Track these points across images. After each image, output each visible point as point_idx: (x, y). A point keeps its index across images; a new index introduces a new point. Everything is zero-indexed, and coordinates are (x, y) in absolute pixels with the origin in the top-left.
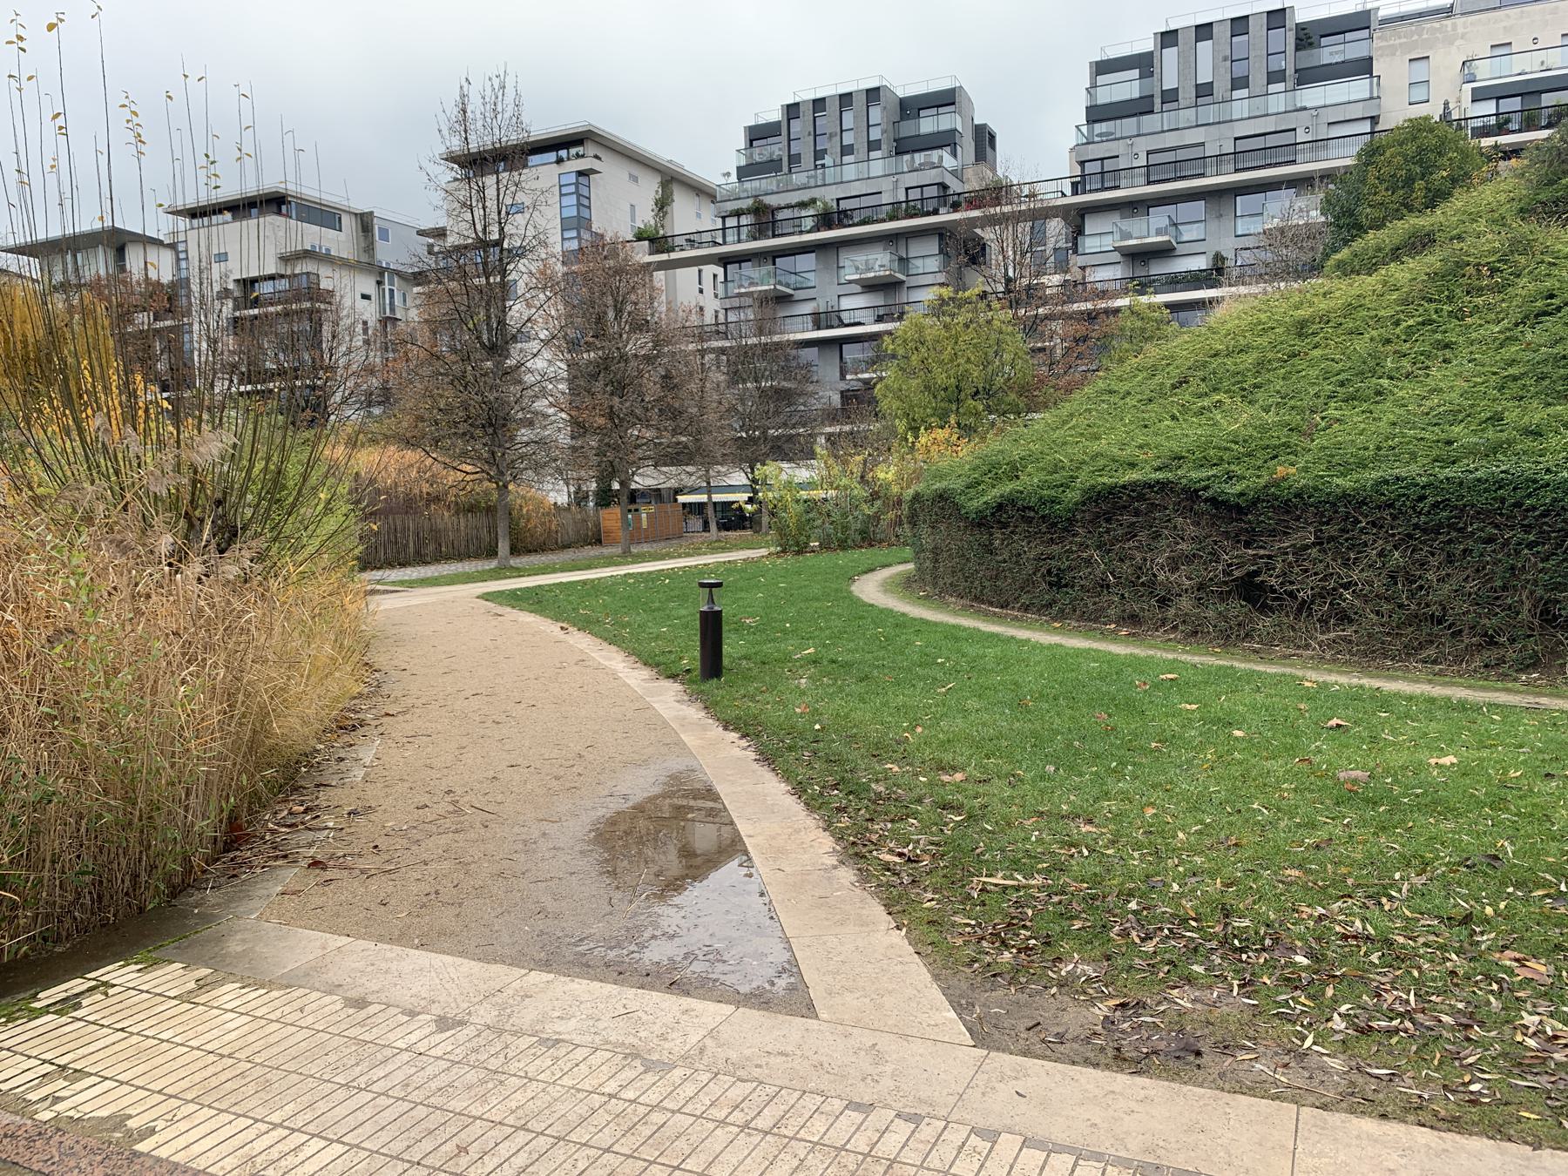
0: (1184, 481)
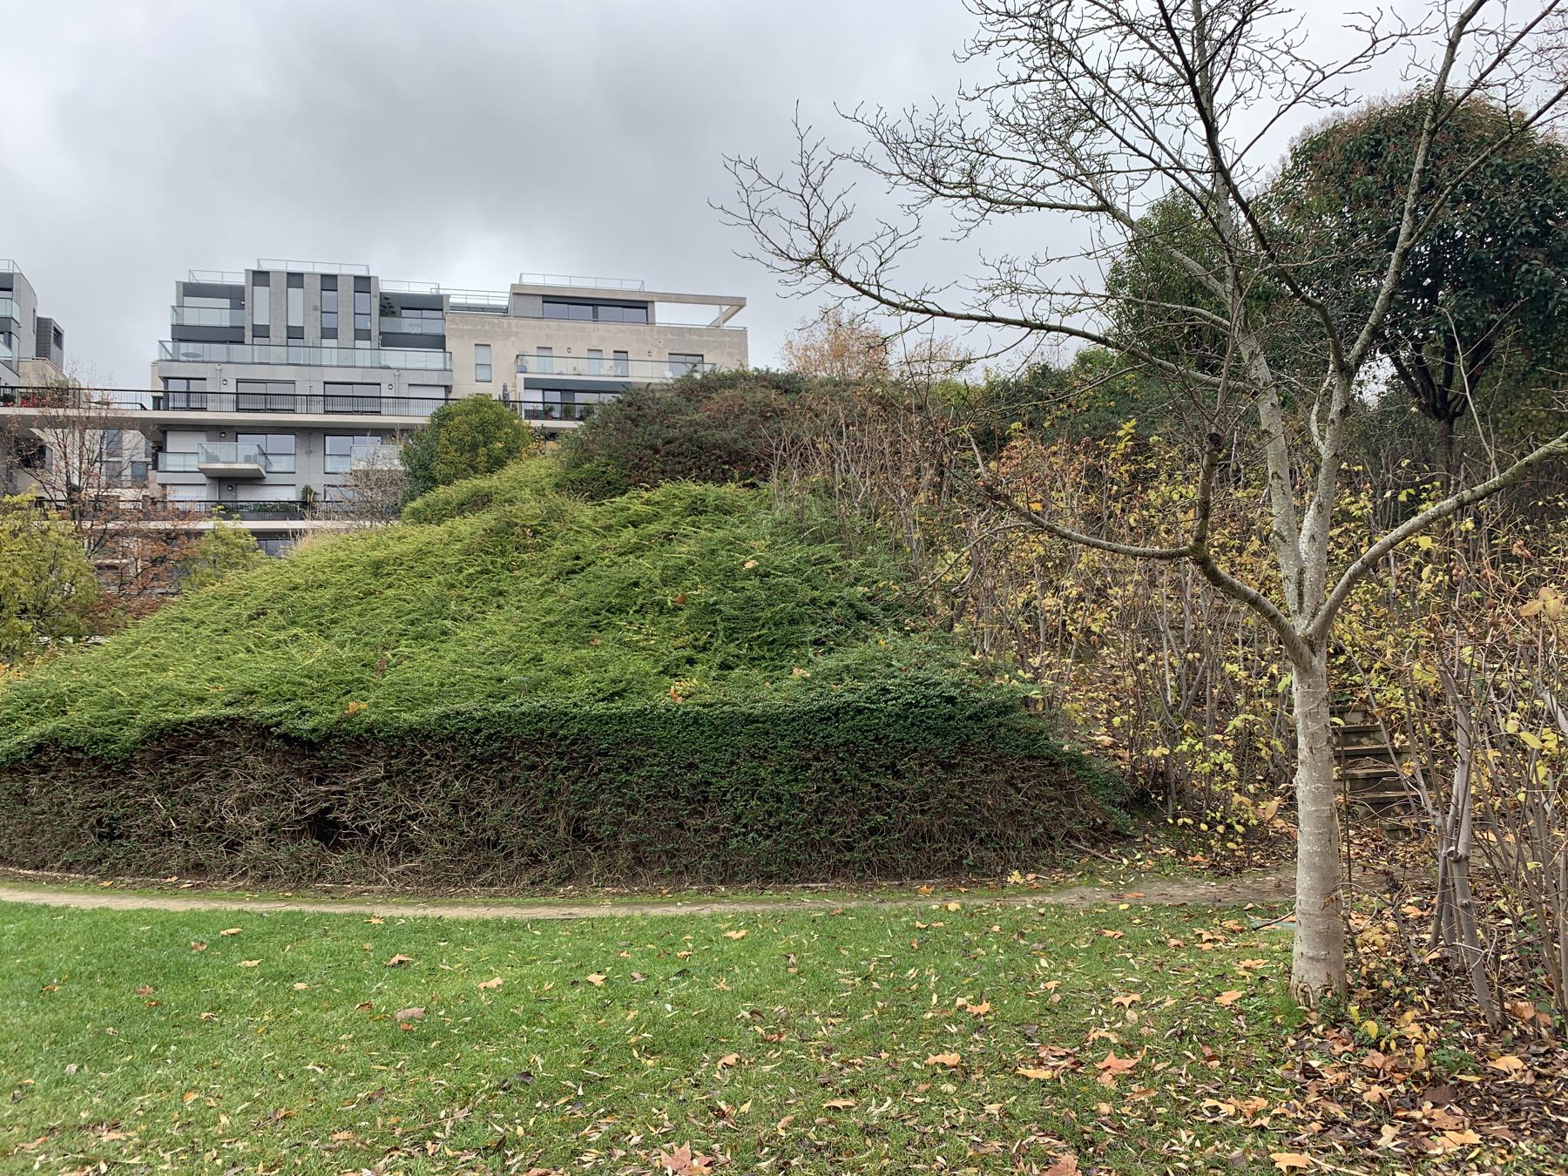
0: (256, 717)
